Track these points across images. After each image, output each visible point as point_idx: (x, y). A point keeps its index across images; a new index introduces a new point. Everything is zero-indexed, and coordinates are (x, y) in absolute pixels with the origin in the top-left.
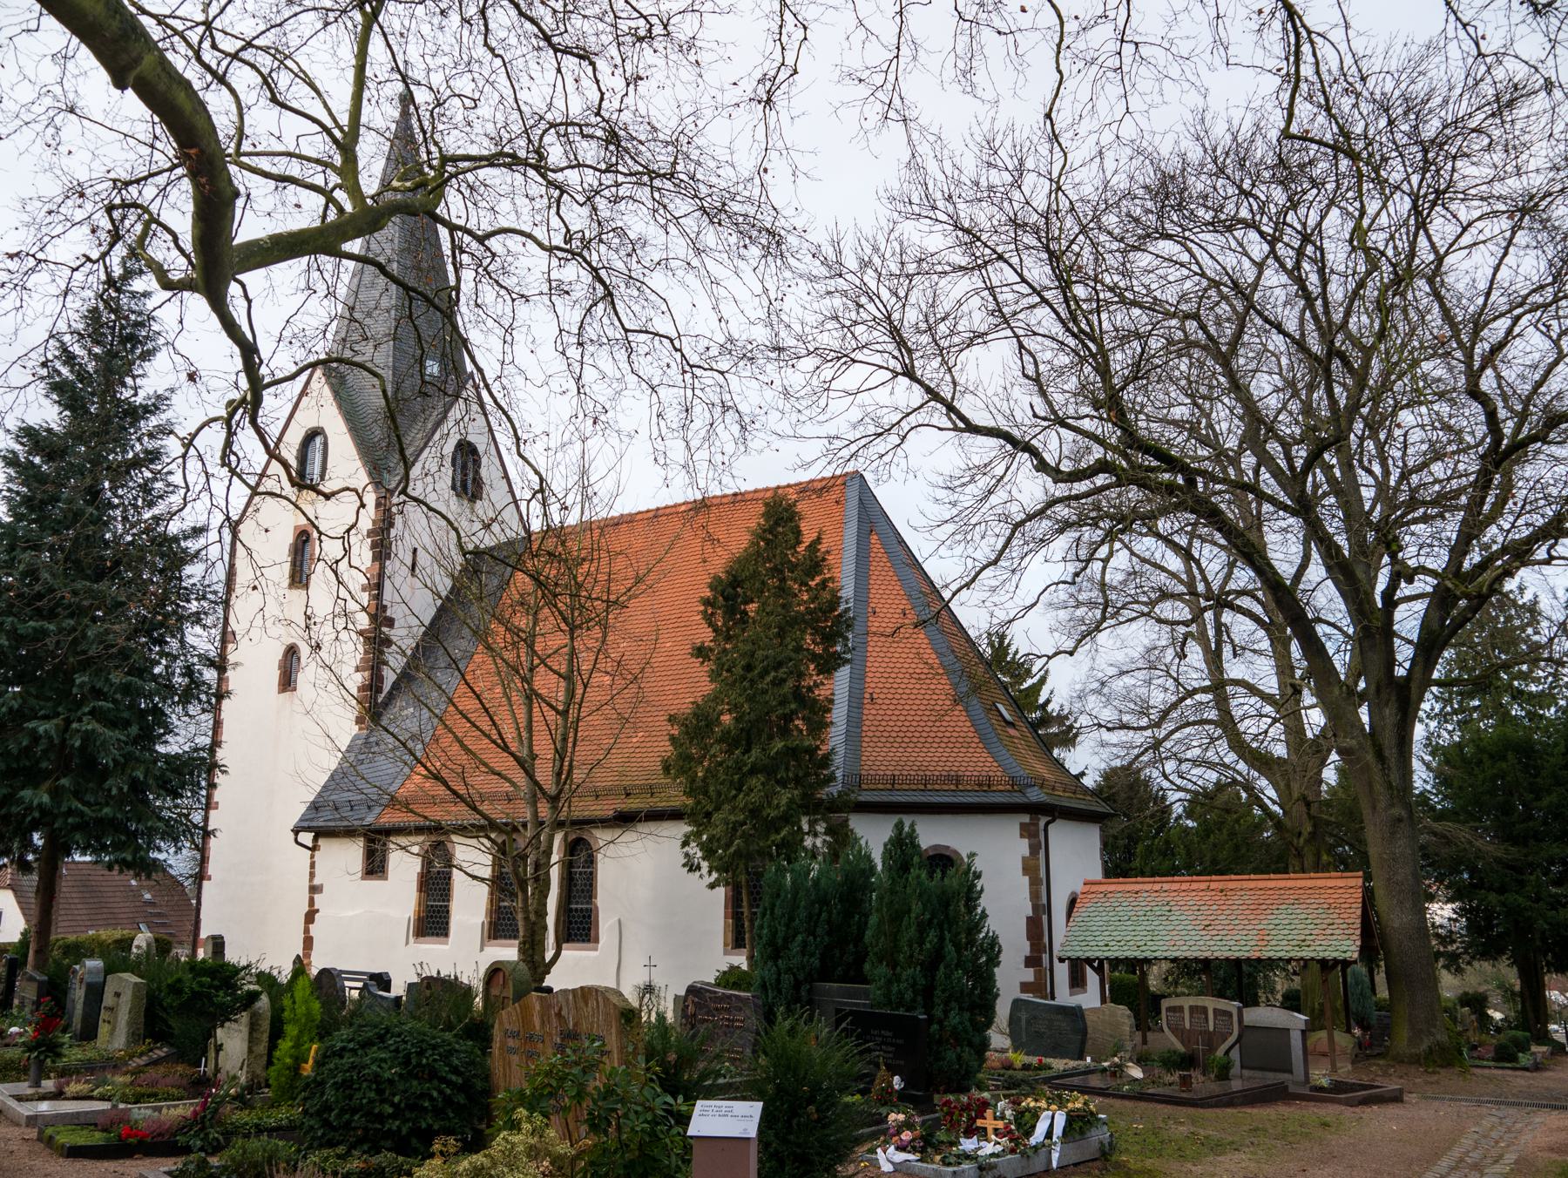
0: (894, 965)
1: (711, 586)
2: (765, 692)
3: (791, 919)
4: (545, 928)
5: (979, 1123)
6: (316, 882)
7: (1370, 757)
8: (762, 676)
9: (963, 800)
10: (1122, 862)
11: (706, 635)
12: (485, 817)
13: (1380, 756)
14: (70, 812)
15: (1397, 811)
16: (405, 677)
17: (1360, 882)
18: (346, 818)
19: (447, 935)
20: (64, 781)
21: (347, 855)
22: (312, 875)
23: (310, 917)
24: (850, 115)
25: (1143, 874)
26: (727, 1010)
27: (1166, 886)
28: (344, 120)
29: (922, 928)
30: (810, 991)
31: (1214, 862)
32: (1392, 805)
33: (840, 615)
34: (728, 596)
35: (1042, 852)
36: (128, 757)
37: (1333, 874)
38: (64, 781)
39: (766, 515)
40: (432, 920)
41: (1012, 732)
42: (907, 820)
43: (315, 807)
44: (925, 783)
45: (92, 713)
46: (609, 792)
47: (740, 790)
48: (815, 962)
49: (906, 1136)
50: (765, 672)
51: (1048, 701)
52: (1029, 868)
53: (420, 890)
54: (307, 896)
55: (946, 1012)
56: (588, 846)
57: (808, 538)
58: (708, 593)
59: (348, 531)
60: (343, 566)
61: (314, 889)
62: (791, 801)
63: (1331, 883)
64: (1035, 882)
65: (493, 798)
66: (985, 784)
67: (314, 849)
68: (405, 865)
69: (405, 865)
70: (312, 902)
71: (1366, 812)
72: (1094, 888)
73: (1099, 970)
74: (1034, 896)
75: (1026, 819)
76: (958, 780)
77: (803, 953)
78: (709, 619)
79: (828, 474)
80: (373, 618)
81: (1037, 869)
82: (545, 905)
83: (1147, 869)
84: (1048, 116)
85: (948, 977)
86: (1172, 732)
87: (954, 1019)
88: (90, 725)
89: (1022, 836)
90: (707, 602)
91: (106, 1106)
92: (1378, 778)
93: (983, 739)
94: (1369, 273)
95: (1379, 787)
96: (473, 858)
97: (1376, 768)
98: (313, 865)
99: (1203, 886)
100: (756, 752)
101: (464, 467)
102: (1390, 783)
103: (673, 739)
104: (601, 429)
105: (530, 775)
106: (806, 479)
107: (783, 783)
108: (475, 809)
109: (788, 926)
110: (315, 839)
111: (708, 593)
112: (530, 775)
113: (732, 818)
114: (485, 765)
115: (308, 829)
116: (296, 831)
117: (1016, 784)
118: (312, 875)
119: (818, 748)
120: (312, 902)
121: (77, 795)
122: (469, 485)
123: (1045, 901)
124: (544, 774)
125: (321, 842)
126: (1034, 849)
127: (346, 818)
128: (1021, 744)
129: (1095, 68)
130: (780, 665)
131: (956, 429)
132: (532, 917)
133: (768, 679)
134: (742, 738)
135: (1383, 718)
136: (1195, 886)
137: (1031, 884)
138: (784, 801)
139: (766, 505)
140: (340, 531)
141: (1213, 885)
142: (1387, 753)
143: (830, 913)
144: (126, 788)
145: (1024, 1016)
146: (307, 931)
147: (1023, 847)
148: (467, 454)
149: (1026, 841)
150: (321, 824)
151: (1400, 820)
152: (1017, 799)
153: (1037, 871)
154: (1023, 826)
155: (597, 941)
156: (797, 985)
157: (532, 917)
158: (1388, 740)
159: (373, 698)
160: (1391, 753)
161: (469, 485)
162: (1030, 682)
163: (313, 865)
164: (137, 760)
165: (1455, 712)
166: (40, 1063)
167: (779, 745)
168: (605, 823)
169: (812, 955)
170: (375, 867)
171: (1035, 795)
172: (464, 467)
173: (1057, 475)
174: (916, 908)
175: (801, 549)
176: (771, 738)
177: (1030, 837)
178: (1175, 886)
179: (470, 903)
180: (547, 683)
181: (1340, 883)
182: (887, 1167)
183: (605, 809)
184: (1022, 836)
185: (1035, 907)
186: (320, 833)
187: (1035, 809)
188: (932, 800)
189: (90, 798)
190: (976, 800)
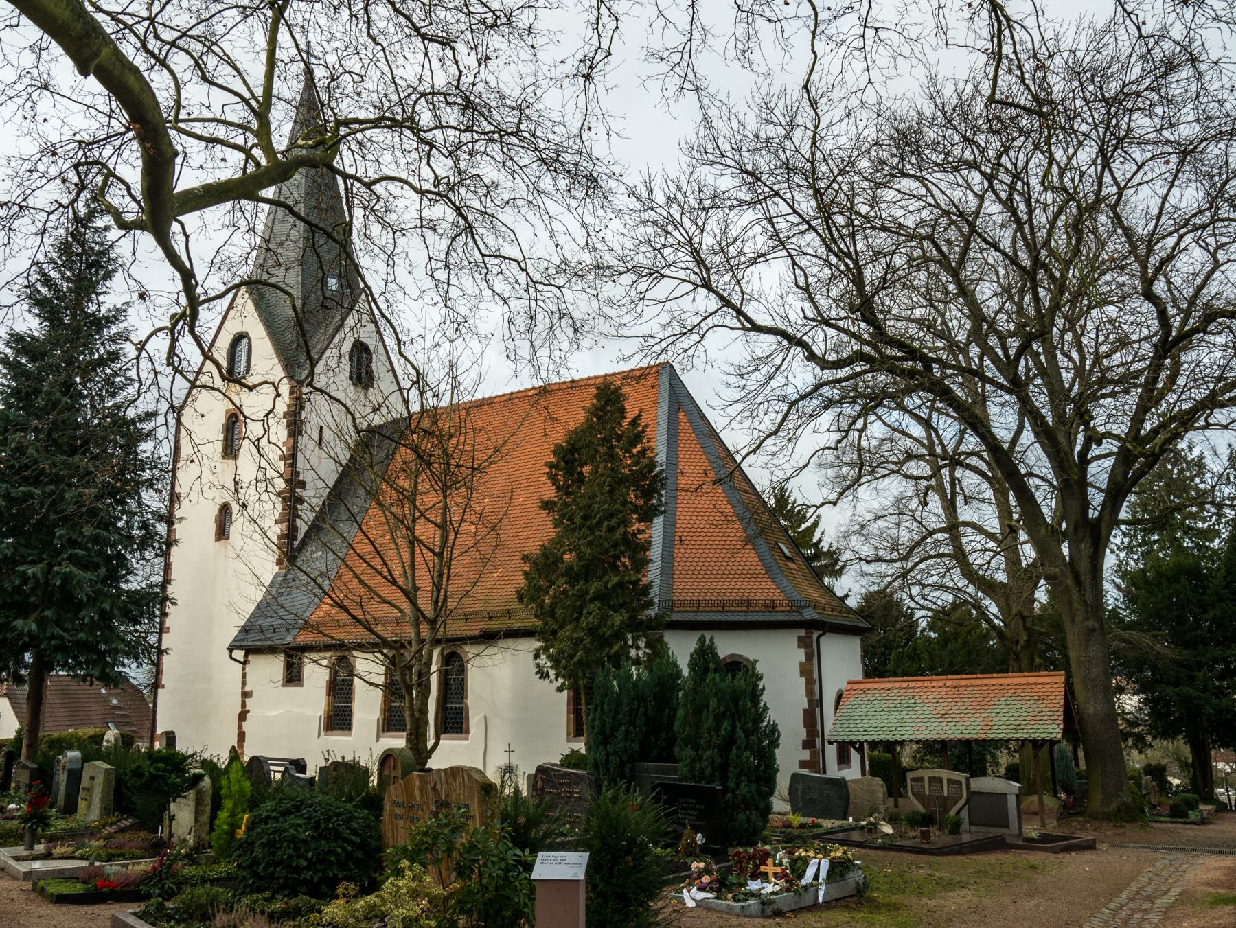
0: (696, 748)
1: (554, 453)
3: (617, 713)
4: (427, 722)
5: (762, 868)
6: (247, 689)
7: (1070, 582)
10: (879, 665)
11: (550, 492)
12: (378, 636)
14: (53, 636)
15: (1091, 623)
16: (315, 528)
19: (350, 729)
20: (47, 613)
22: (244, 684)
23: (243, 716)
25: (895, 675)
26: (567, 784)
27: (912, 684)
28: (259, 92)
29: (719, 718)
30: (632, 769)
31: (951, 664)
32: (1088, 619)
34: (568, 459)
35: (815, 659)
39: (597, 397)
41: (791, 565)
43: (245, 630)
44: (723, 606)
48: (636, 746)
49: (706, 879)
51: (820, 540)
52: (805, 671)
53: (329, 694)
54: (240, 699)
55: (738, 784)
56: (460, 658)
57: (631, 414)
58: (552, 459)
59: (267, 415)
60: (264, 442)
61: (246, 695)
64: (809, 683)
65: (385, 622)
66: (771, 607)
67: (245, 663)
68: (316, 674)
69: (316, 674)
70: (244, 704)
72: (856, 686)
74: (810, 693)
75: (802, 633)
76: (749, 603)
77: (626, 739)
78: (553, 478)
83: (899, 671)
85: (739, 757)
87: (744, 789)
89: (799, 646)
90: (551, 465)
91: (84, 864)
92: (1076, 597)
93: (768, 570)
97: (1074, 589)
98: (244, 676)
99: (941, 683)
105: (414, 603)
108: (370, 630)
110: (246, 655)
111: (552, 459)
112: (414, 603)
115: (240, 648)
116: (231, 649)
117: (795, 606)
118: (244, 684)
120: (244, 704)
121: (58, 623)
122: (363, 377)
123: (817, 697)
124: (425, 602)
125: (250, 657)
126: (809, 656)
128: (798, 575)
129: (844, 48)
131: (744, 328)
132: (417, 715)
135: (1080, 551)
136: (934, 684)
138: (618, 623)
139: (598, 388)
141: (948, 683)
143: (646, 708)
145: (800, 787)
146: (240, 727)
147: (801, 655)
148: (361, 351)
150: (251, 643)
151: (1093, 630)
152: (795, 617)
153: (811, 673)
154: (800, 639)
155: (468, 732)
156: (622, 765)
157: (417, 715)
158: (1084, 567)
159: (290, 544)
161: (363, 377)
163: (244, 676)
166: (33, 832)
169: (633, 741)
170: (293, 677)
171: (809, 614)
173: (824, 364)
174: (713, 703)
180: (425, 531)
183: (473, 629)
184: (799, 646)
185: (810, 702)
186: (249, 651)
187: (809, 625)
189: (68, 625)
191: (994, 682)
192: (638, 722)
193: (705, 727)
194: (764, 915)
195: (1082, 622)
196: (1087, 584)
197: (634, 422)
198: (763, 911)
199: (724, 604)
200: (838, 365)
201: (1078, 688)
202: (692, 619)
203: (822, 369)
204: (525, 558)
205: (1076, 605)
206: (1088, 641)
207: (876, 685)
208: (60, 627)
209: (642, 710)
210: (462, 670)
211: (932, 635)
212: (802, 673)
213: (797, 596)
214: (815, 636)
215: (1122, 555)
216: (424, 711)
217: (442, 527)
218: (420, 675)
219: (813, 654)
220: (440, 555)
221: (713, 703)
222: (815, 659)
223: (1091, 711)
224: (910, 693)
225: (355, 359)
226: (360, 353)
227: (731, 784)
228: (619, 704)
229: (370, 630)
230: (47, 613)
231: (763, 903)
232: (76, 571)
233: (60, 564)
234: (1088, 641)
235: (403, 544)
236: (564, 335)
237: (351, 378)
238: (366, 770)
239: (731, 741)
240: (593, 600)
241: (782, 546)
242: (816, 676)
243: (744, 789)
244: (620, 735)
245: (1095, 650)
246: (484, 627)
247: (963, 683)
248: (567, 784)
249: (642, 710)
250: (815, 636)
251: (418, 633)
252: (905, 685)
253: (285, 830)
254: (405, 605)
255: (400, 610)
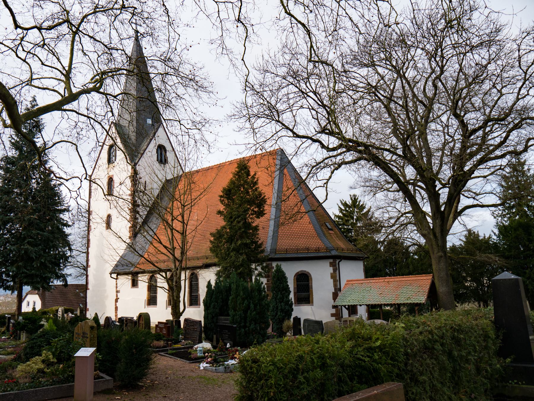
1: (223, 192)
3: (211, 298)
4: (180, 302)
5: (235, 356)
6: (118, 289)
7: (432, 237)
10: (371, 273)
11: (222, 208)
12: (157, 267)
13: (435, 235)
14: (23, 273)
15: (440, 254)
16: (145, 222)
19: (156, 305)
20: (20, 264)
21: (125, 281)
22: (117, 287)
23: (116, 300)
24: (214, 52)
25: (399, 275)
26: (193, 325)
27: (371, 281)
28: (67, 69)
29: (243, 299)
31: (422, 270)
32: (439, 252)
33: (262, 198)
34: (228, 194)
38: (20, 264)
39: (238, 167)
40: (152, 301)
41: (331, 232)
43: (116, 266)
44: (297, 250)
48: (217, 310)
49: (209, 360)
50: (235, 219)
51: (372, 217)
52: (333, 276)
53: (148, 291)
54: (115, 294)
55: (250, 324)
57: (252, 174)
58: (222, 194)
59: (79, 189)
61: (117, 292)
62: (243, 260)
63: (422, 278)
64: (335, 281)
65: (161, 261)
66: (318, 250)
67: (117, 279)
68: (143, 281)
69: (143, 281)
70: (117, 296)
71: (432, 255)
72: (349, 282)
74: (335, 285)
75: (332, 261)
76: (308, 249)
77: (214, 308)
78: (222, 201)
79: (248, 155)
83: (400, 273)
84: (243, 60)
85: (251, 314)
86: (398, 228)
88: (27, 246)
90: (221, 196)
92: (434, 243)
93: (318, 235)
95: (434, 246)
96: (161, 282)
99: (383, 280)
100: (233, 245)
101: (161, 154)
103: (211, 241)
104: (213, 136)
105: (173, 255)
106: (242, 157)
107: (241, 254)
108: (154, 265)
110: (117, 276)
111: (222, 194)
112: (173, 255)
114: (160, 251)
115: (114, 273)
116: (111, 274)
117: (328, 250)
118: (117, 287)
119: (258, 241)
120: (117, 296)
122: (162, 160)
123: (339, 287)
124: (178, 254)
126: (335, 270)
129: (286, 31)
130: (239, 217)
131: (294, 137)
132: (175, 298)
134: (230, 240)
136: (380, 281)
138: (241, 259)
139: (238, 164)
140: (76, 189)
144: (39, 265)
145: (307, 324)
146: (116, 305)
147: (331, 270)
148: (161, 149)
149: (332, 268)
150: (118, 271)
151: (441, 257)
152: (328, 254)
153: (336, 277)
154: (331, 263)
156: (213, 317)
157: (175, 298)
160: (438, 234)
161: (162, 160)
162: (365, 210)
165: (507, 214)
167: (239, 242)
168: (201, 268)
170: (134, 284)
171: (334, 253)
172: (161, 154)
173: (328, 149)
175: (249, 177)
176: (237, 240)
178: (374, 281)
179: (162, 296)
180: (177, 225)
181: (425, 278)
182: (202, 368)
183: (200, 263)
184: (330, 266)
185: (335, 289)
186: (118, 274)
187: (334, 257)
188: (299, 256)
191: (403, 279)
192: (219, 301)
194: (226, 372)
195: (437, 253)
197: (253, 177)
198: (225, 371)
199: (297, 250)
200: (334, 149)
201: (436, 281)
202: (283, 256)
204: (211, 234)
205: (434, 246)
207: (374, 281)
210: (197, 280)
211: (416, 257)
212: (332, 277)
214: (337, 262)
215: (500, 219)
217: (183, 222)
218: (176, 282)
221: (242, 293)
224: (370, 285)
225: (159, 152)
226: (161, 149)
232: (30, 247)
233: (24, 245)
234: (439, 261)
235: (169, 231)
236: (204, 150)
238: (201, 321)
240: (232, 251)
241: (327, 224)
242: (338, 278)
243: (252, 326)
244: (212, 307)
245: (442, 265)
246: (205, 262)
247: (391, 280)
248: (193, 325)
249: (221, 297)
250: (337, 262)
251: (175, 266)
253: (37, 343)
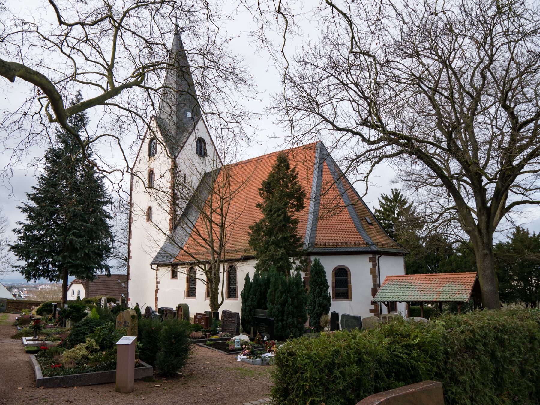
0: (273, 304)
2: (275, 219)
3: (250, 291)
4: (218, 294)
5: (272, 349)
6: (158, 280)
7: (476, 233)
8: (274, 214)
9: (327, 251)
10: (412, 269)
11: (261, 201)
14: (68, 262)
15: (486, 251)
17: (475, 275)
18: (167, 261)
20: (66, 254)
21: (165, 273)
22: (157, 278)
23: (157, 291)
24: (253, 45)
25: (441, 272)
27: (412, 278)
28: (109, 63)
29: (282, 293)
30: (254, 312)
31: (466, 268)
32: (484, 249)
34: (268, 187)
35: (377, 267)
36: (84, 246)
37: (453, 273)
39: (278, 160)
40: (191, 292)
41: (371, 227)
42: (318, 257)
43: (157, 257)
44: (336, 245)
45: (73, 234)
46: (240, 250)
47: (267, 249)
48: (255, 303)
49: (247, 352)
51: (414, 212)
52: (372, 272)
53: (187, 282)
55: (288, 318)
56: (194, 269)
57: (292, 167)
58: (261, 187)
60: (121, 191)
62: (283, 253)
64: (374, 277)
65: (199, 253)
66: (357, 245)
67: (157, 270)
68: (183, 273)
69: (183, 273)
70: (157, 286)
72: (389, 278)
73: (387, 305)
74: (374, 281)
75: (371, 256)
76: (347, 244)
77: (252, 300)
78: (261, 194)
79: (287, 148)
80: (173, 197)
81: (375, 272)
82: (218, 287)
83: (443, 270)
84: (282, 52)
85: (288, 308)
87: (290, 320)
89: (370, 262)
90: (261, 189)
91: (40, 342)
92: (479, 240)
93: (358, 230)
94: (480, 63)
97: (478, 237)
98: (157, 275)
101: (201, 147)
102: (483, 242)
104: (252, 128)
105: (212, 248)
107: (281, 248)
108: (193, 257)
109: (248, 293)
110: (157, 267)
111: (261, 187)
113: (264, 259)
114: (199, 243)
115: (155, 264)
116: (151, 265)
117: (368, 245)
118: (157, 278)
119: (296, 235)
120: (157, 286)
121: (70, 258)
122: (202, 153)
123: (378, 283)
124: (216, 246)
125: (159, 268)
126: (374, 266)
127: (167, 261)
128: (374, 232)
129: (327, 22)
130: (279, 210)
132: (214, 290)
133: (276, 215)
134: (270, 233)
135: (482, 220)
136: (421, 277)
137: (373, 277)
138: (280, 253)
140: (118, 182)
141: (427, 277)
142: (483, 232)
143: (261, 289)
144: (83, 255)
145: (345, 320)
146: (156, 295)
147: (370, 265)
148: (201, 142)
150: (158, 263)
151: (487, 254)
152: (368, 249)
153: (375, 273)
154: (370, 258)
155: (351, 298)
156: (251, 310)
157: (214, 290)
158: (483, 227)
159: (174, 223)
160: (484, 231)
161: (202, 153)
163: (157, 275)
164: (87, 247)
166: (36, 331)
168: (238, 260)
169: (255, 301)
170: (174, 275)
171: (373, 248)
172: (201, 147)
173: (369, 142)
174: (280, 287)
175: (289, 171)
177: (372, 262)
178: (415, 278)
180: (216, 218)
181: (468, 276)
184: (370, 262)
185: (375, 285)
186: (159, 265)
189: (73, 258)
190: (335, 250)
193: (277, 296)
195: (482, 251)
196: (485, 235)
198: (262, 363)
199: (336, 244)
203: (368, 144)
205: (479, 243)
206: (484, 259)
208: (71, 259)
209: (259, 290)
210: (235, 272)
212: (371, 273)
213: (369, 240)
214: (377, 257)
216: (217, 289)
217: (222, 215)
219: (376, 265)
220: (221, 226)
221: (280, 287)
222: (377, 267)
223: (485, 289)
224: (410, 281)
227: (285, 318)
228: (251, 287)
229: (193, 257)
230: (66, 254)
231: (262, 360)
232: (75, 238)
234: (484, 259)
235: (208, 223)
237: (197, 153)
238: (238, 314)
239: (286, 301)
241: (367, 219)
242: (377, 274)
243: (290, 320)
244: (250, 299)
246: (243, 255)
247: (433, 277)
249: (259, 290)
250: (377, 257)
252: (409, 278)
254: (210, 249)
255: (207, 249)
